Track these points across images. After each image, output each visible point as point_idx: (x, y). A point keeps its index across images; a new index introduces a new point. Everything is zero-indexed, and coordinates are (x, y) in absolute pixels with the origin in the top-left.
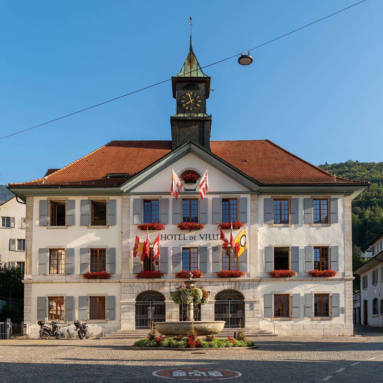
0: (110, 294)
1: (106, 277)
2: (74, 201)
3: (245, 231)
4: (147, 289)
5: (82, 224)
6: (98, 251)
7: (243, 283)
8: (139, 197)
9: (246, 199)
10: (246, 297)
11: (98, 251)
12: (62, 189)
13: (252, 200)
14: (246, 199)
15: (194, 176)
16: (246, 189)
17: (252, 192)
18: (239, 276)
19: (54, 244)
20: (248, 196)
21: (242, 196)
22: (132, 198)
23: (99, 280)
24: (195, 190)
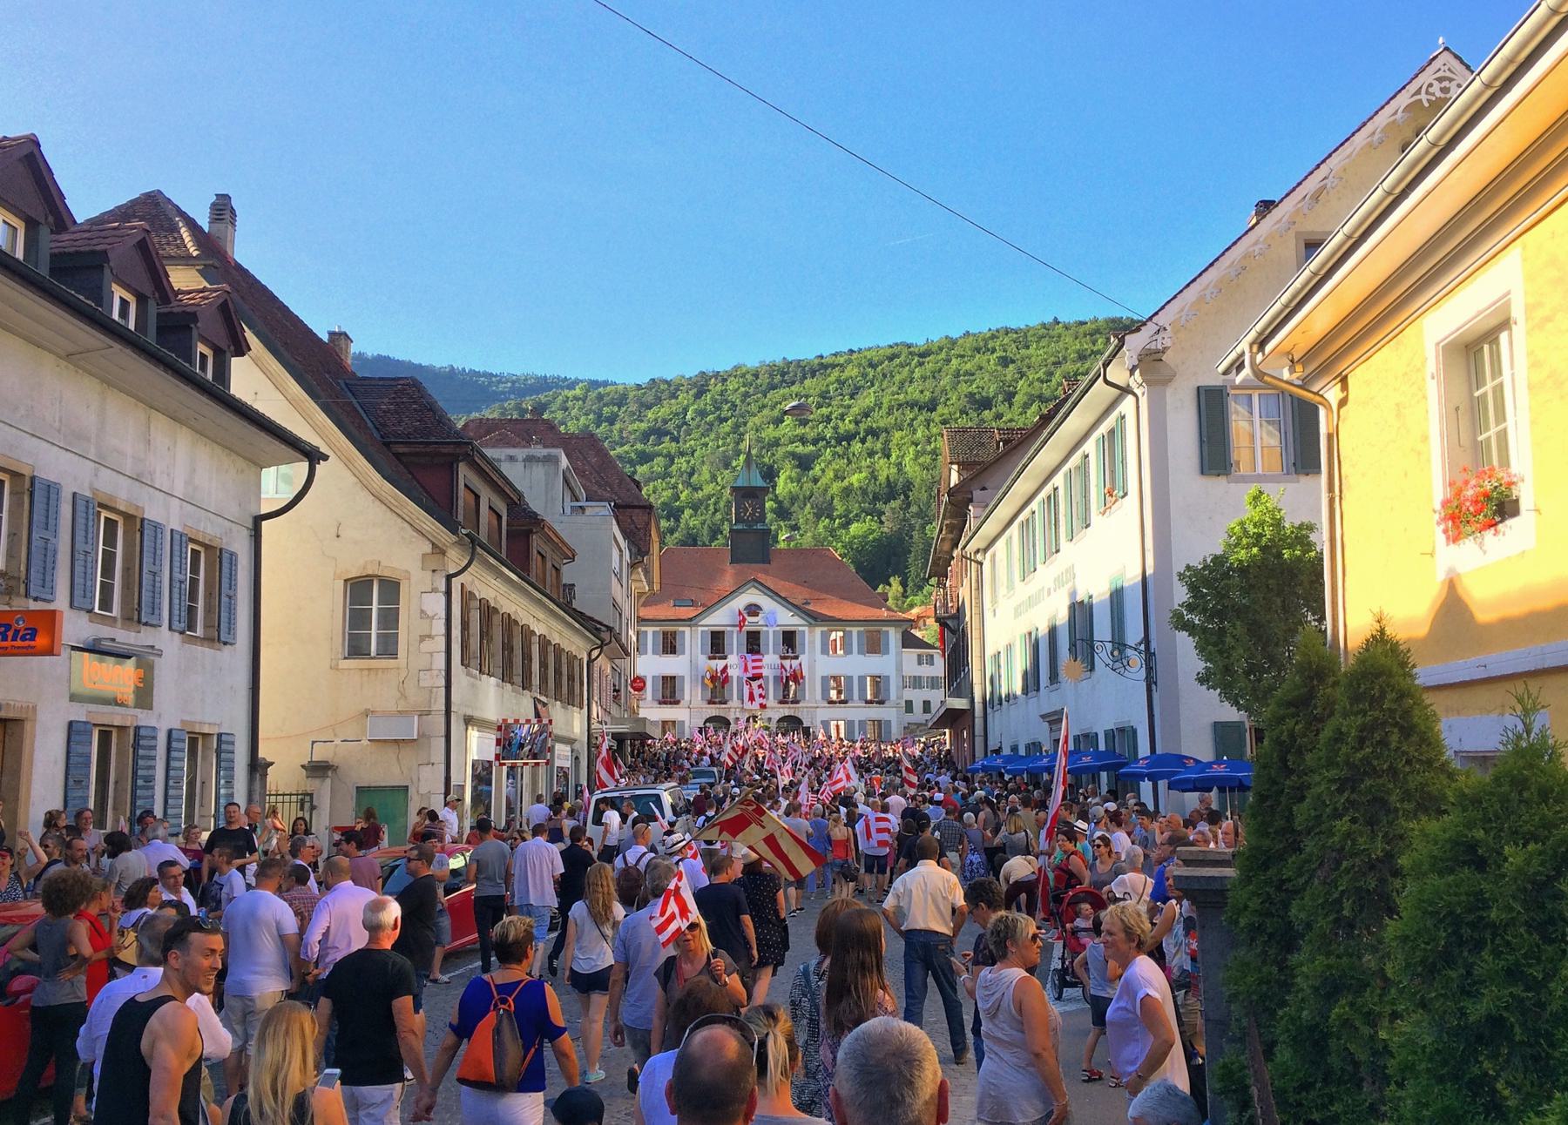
8: (706, 629)
13: (810, 632)
17: (810, 625)
20: (806, 629)
21: (800, 628)
22: (700, 629)
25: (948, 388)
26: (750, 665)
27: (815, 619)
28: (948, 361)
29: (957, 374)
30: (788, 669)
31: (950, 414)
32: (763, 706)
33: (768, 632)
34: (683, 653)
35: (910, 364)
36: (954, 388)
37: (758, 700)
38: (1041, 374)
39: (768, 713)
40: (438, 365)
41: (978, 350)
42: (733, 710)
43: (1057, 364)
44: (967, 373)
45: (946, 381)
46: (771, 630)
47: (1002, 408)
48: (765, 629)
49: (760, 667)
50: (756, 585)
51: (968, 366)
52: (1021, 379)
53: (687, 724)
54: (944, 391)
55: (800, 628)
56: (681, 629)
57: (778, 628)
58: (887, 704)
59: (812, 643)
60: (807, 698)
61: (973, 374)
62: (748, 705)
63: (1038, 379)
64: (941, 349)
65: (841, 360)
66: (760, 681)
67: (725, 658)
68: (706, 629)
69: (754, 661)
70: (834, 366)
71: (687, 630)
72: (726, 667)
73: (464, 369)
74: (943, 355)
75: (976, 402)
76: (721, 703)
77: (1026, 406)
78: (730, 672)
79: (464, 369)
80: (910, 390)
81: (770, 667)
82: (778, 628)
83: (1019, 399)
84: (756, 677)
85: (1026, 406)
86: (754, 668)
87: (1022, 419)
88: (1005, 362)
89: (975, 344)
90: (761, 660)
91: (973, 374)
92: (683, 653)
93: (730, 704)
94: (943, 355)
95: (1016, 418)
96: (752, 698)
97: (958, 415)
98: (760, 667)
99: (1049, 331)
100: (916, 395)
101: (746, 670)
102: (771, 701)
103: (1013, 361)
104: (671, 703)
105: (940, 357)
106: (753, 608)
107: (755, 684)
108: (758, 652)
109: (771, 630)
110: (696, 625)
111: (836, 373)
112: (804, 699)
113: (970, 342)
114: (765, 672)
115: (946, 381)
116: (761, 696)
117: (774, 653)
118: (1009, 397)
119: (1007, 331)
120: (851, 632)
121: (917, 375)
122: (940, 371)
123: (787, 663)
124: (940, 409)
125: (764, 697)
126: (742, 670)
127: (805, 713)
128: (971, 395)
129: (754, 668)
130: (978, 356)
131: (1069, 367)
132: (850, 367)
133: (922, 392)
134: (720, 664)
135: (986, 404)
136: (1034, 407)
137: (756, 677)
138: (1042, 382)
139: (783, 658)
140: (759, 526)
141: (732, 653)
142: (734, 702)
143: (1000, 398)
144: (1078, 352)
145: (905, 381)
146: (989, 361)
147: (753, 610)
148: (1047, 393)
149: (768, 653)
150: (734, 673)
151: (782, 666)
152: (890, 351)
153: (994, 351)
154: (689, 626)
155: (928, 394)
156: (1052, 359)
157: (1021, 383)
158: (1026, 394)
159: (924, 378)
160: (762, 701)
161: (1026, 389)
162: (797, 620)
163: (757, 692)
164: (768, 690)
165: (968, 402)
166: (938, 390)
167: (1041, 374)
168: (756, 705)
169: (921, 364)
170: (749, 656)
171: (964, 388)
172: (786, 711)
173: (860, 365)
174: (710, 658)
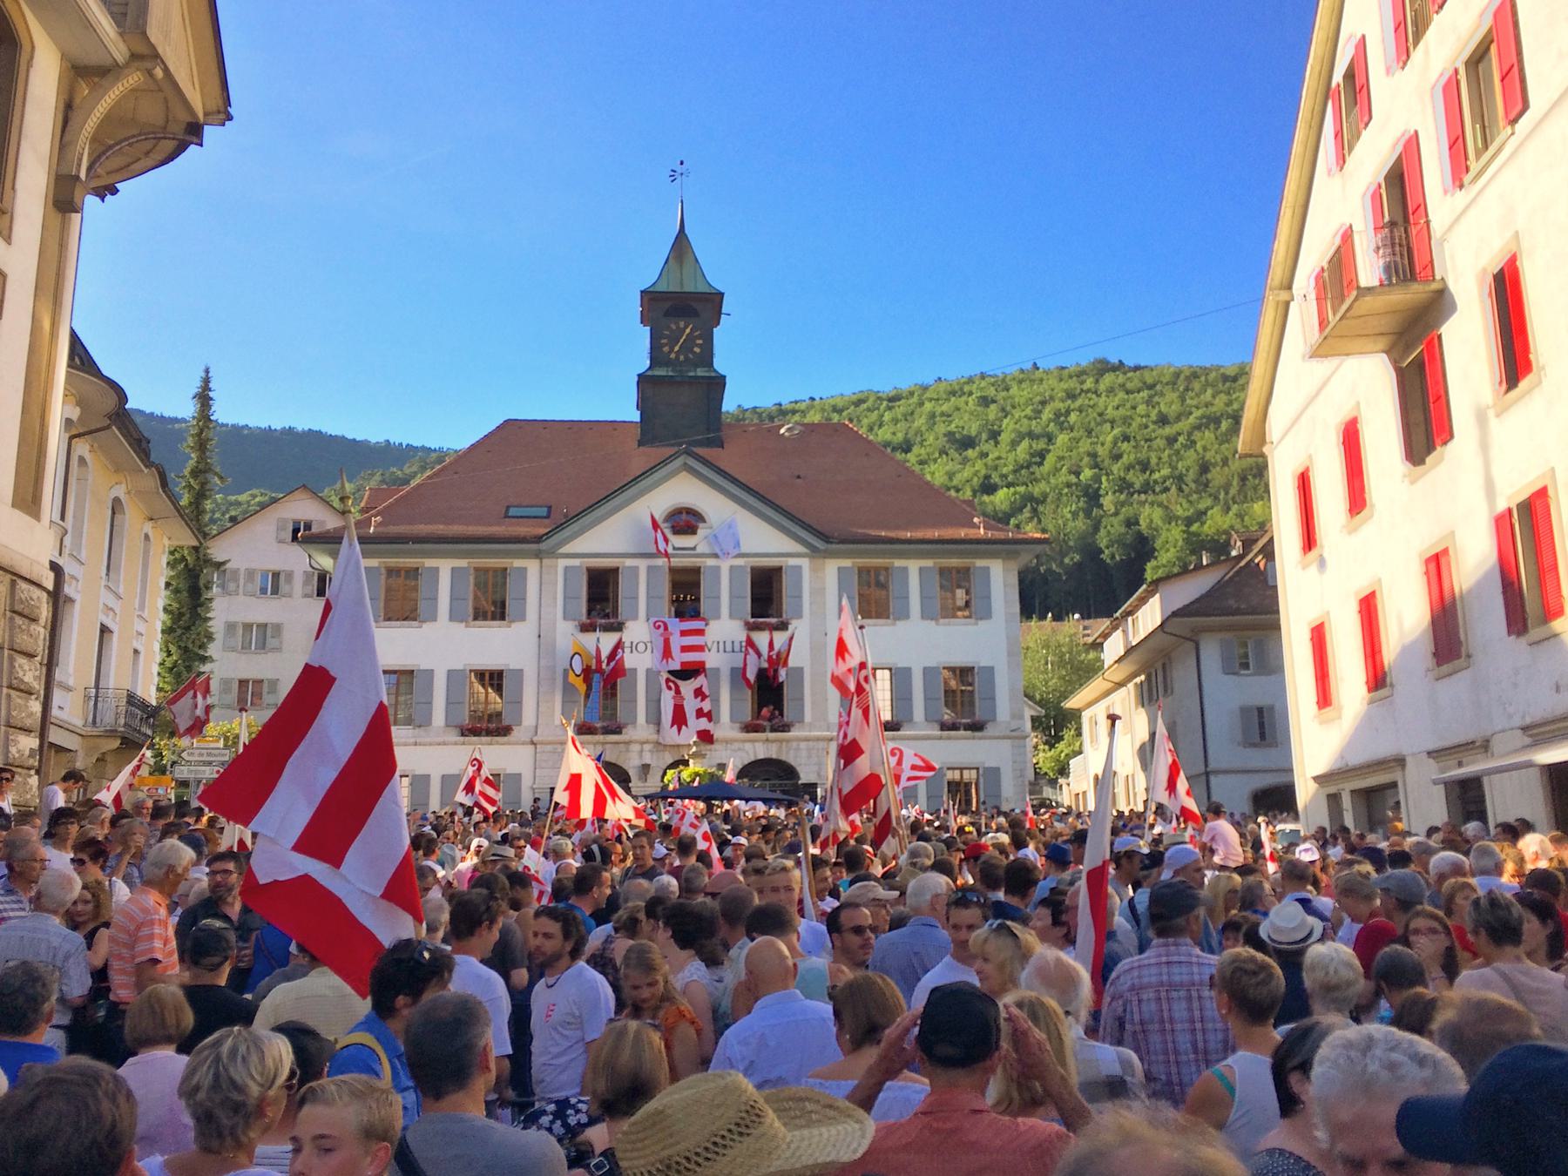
0: (511, 769)
1: (977, 727)
2: (437, 569)
3: (39, 586)
4: (761, 756)
5: (454, 616)
6: (970, 688)
7: (794, 744)
8: (576, 562)
9: (800, 568)
10: (802, 775)
11: (970, 688)
12: (417, 546)
13: (813, 570)
14: (800, 568)
15: (691, 519)
16: (800, 549)
17: (814, 552)
18: (898, 730)
19: (490, 662)
20: (805, 563)
21: (792, 562)
22: (562, 563)
23: (489, 738)
24: (694, 548)
25: (923, 429)
26: (677, 642)
27: (826, 538)
28: (921, 404)
29: (932, 416)
30: (764, 649)
31: (928, 454)
32: (706, 737)
33: (717, 569)
34: (522, 618)
35: (878, 409)
36: (930, 429)
37: (695, 724)
38: (1028, 411)
39: (717, 753)
40: (373, 440)
41: (953, 393)
42: (635, 748)
43: (1043, 403)
44: (943, 414)
45: (920, 422)
46: (725, 565)
47: (986, 447)
48: (711, 562)
49: (700, 648)
50: (692, 462)
51: (945, 408)
52: (1006, 417)
53: (526, 782)
54: (919, 432)
55: (792, 562)
56: (517, 563)
57: (740, 562)
58: (990, 730)
59: (819, 592)
60: (808, 718)
61: (949, 416)
62: (671, 735)
63: (1025, 417)
64: (912, 394)
65: (803, 406)
66: (700, 681)
67: (619, 627)
68: (576, 562)
69: (684, 633)
70: (794, 412)
71: (532, 566)
72: (619, 645)
73: (401, 444)
74: (915, 399)
75: (956, 441)
76: (607, 731)
77: (1014, 444)
78: (630, 660)
79: (401, 444)
80: (880, 432)
81: (722, 647)
82: (740, 562)
83: (1005, 438)
84: (689, 671)
85: (1014, 444)
86: (685, 649)
87: (1011, 457)
88: (985, 401)
89: (949, 388)
90: (700, 632)
91: (949, 416)
92: (522, 618)
93: (629, 734)
94: (915, 399)
95: (1004, 455)
96: (679, 719)
97: (937, 455)
98: (700, 648)
99: (1030, 376)
100: (888, 437)
101: (667, 653)
102: (725, 728)
103: (994, 401)
104: (489, 733)
105: (911, 401)
106: (684, 516)
107: (687, 687)
108: (696, 615)
109: (725, 565)
110: (552, 554)
111: (797, 418)
112: (801, 721)
113: (942, 386)
114: (712, 659)
115: (920, 422)
116: (700, 713)
117: (731, 616)
118: (994, 435)
119: (983, 376)
120: (905, 569)
121: (887, 416)
122: (912, 413)
123: (761, 639)
124: (916, 450)
125: (709, 716)
126: (658, 654)
127: (804, 754)
128: (950, 435)
129: (685, 649)
130: (953, 399)
131: (1058, 405)
132: (812, 412)
133: (894, 434)
134: (607, 641)
135: (967, 443)
136: (1025, 444)
137: (689, 671)
138: (1030, 419)
139: (752, 627)
140: (700, 372)
141: (635, 618)
142: (640, 729)
143: (984, 436)
144: (1066, 391)
145: (874, 424)
146: (967, 403)
147: (685, 521)
148: (1038, 430)
149: (718, 617)
150: (641, 661)
151: (750, 643)
152: (855, 398)
153: (971, 394)
154: (538, 555)
155: (900, 436)
156: (1038, 398)
157: (1006, 421)
158: (1014, 430)
159: (895, 421)
160: (703, 724)
161: (1012, 426)
162: (789, 545)
163: (691, 705)
164: (716, 701)
165: (948, 442)
166: (911, 433)
167: (1028, 411)
168: (689, 736)
169: (890, 408)
170: (676, 626)
171: (941, 428)
172: (760, 747)
173: (823, 410)
174: (586, 628)
